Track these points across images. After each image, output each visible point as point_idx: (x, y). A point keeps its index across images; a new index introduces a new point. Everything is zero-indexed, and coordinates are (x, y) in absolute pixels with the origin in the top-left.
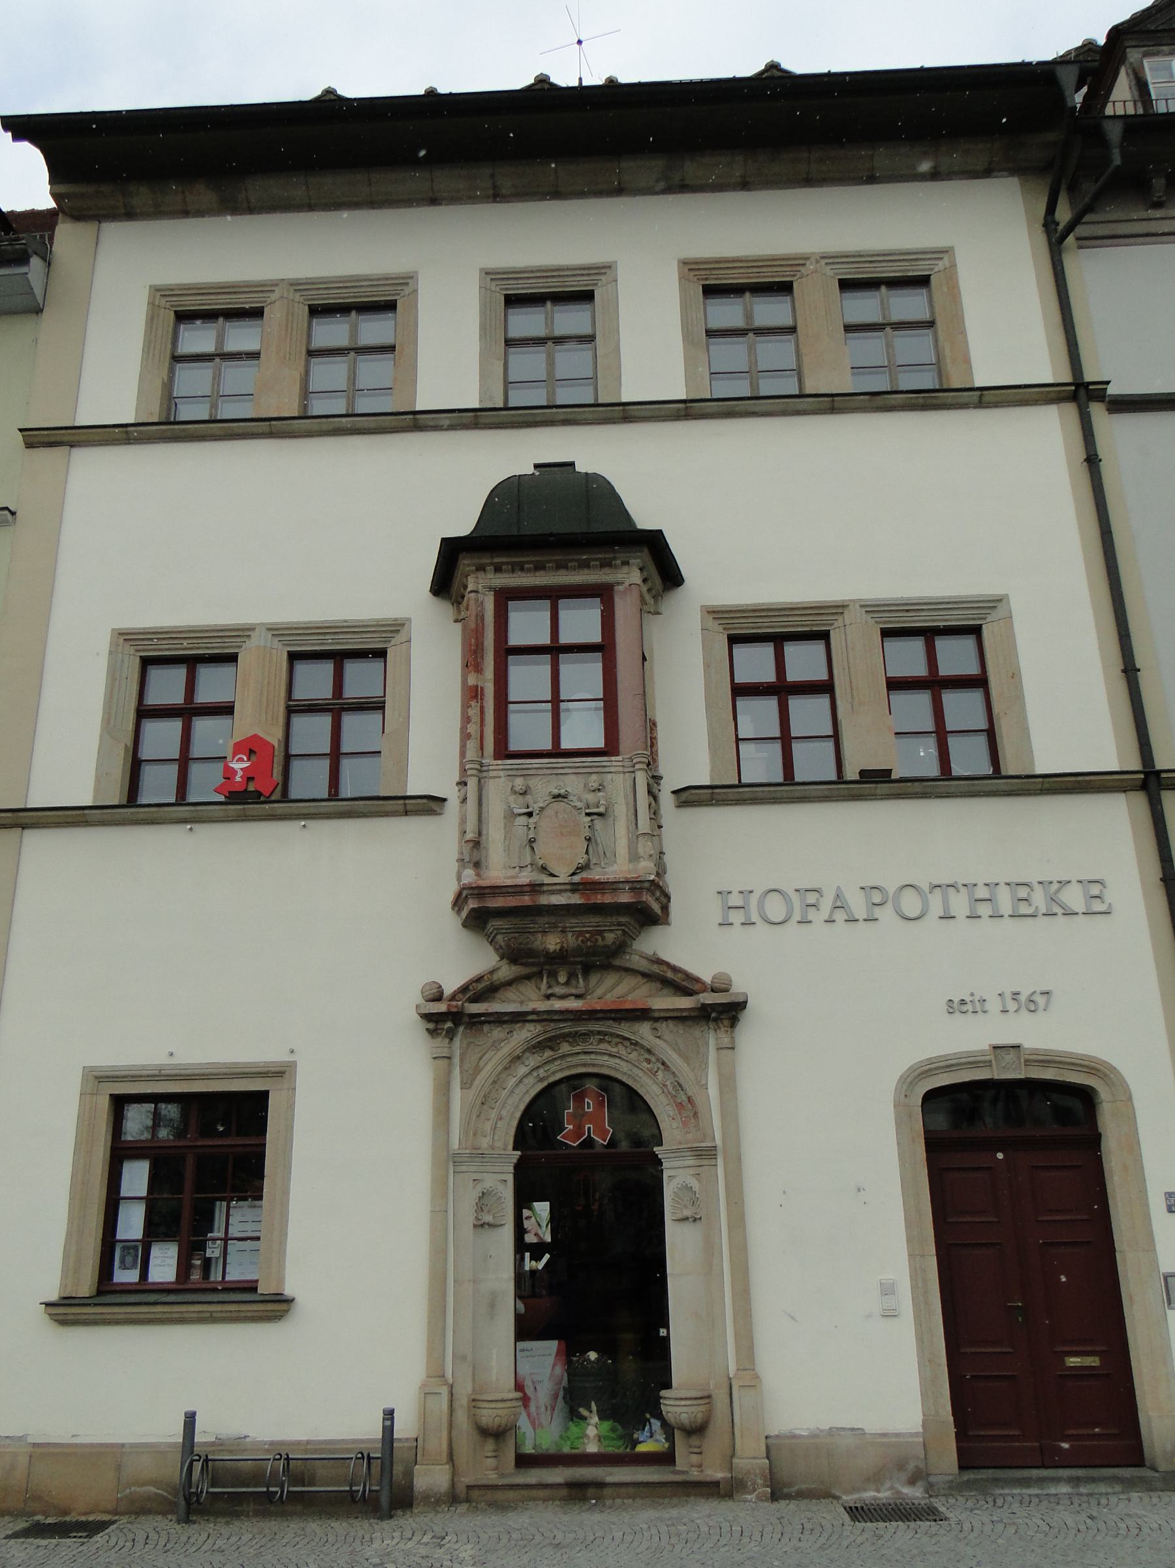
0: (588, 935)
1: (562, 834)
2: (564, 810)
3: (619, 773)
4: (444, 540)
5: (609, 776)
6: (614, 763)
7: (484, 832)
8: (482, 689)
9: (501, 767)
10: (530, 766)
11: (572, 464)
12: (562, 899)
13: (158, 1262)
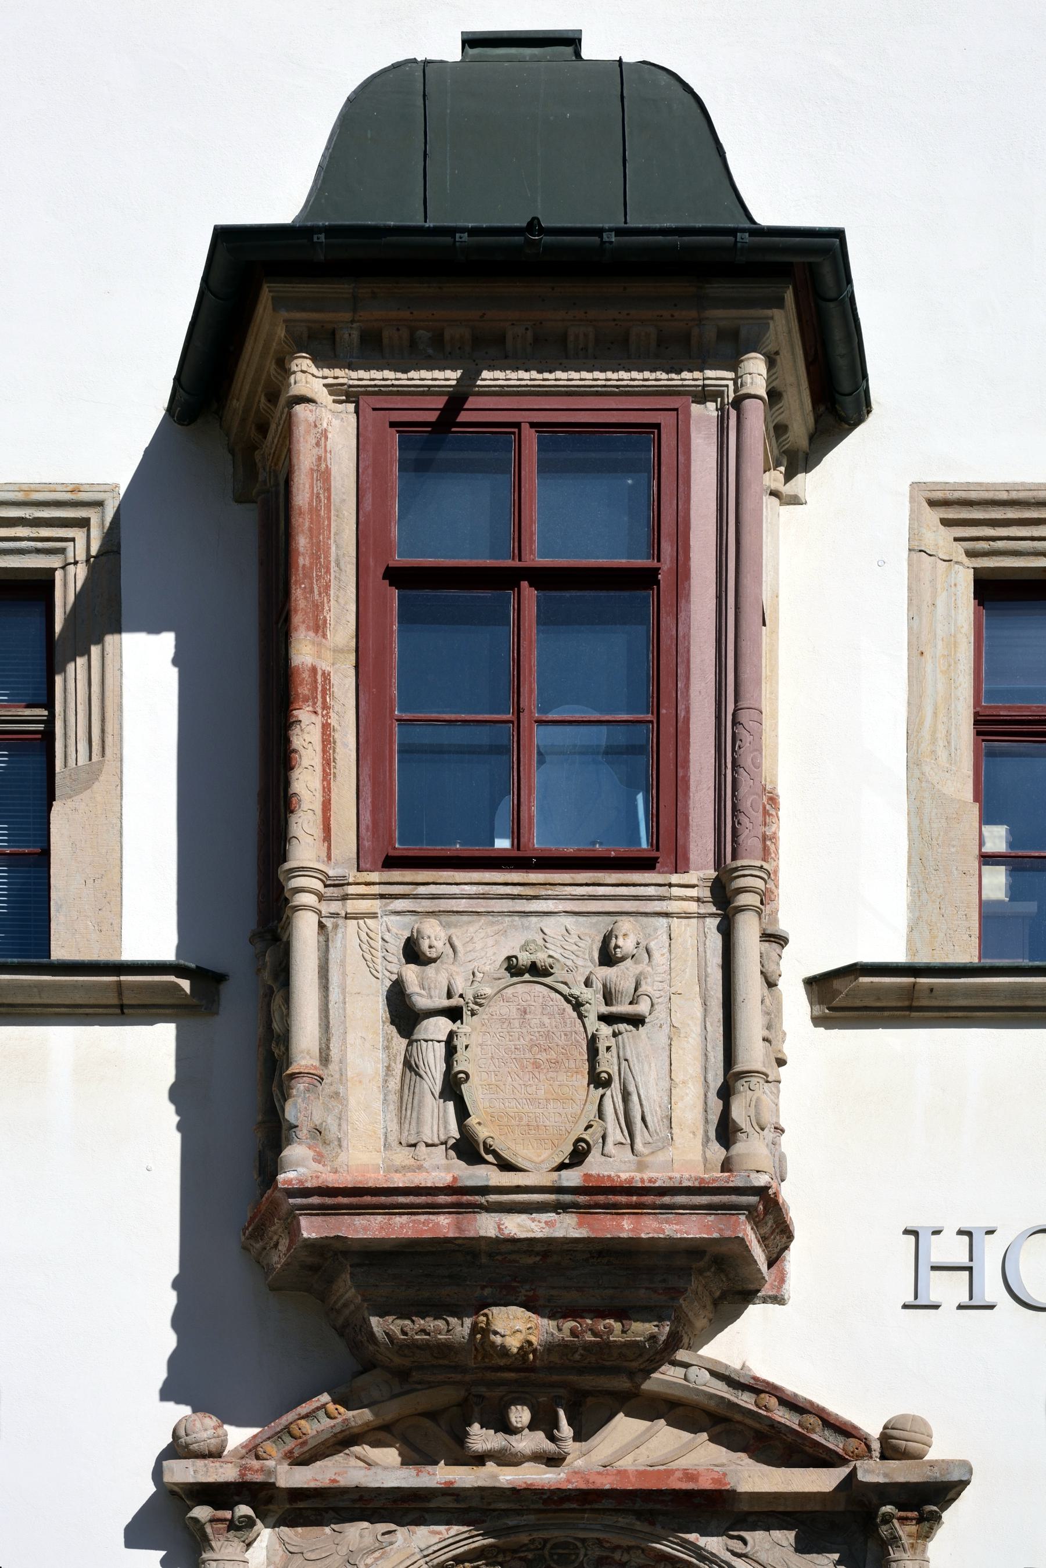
2: (544, 1006)
3: (687, 916)
4: (839, 234)
6: (676, 891)
7: (335, 1052)
8: (326, 676)
11: (571, 41)
12: (533, 1225)
13: (801, 1472)
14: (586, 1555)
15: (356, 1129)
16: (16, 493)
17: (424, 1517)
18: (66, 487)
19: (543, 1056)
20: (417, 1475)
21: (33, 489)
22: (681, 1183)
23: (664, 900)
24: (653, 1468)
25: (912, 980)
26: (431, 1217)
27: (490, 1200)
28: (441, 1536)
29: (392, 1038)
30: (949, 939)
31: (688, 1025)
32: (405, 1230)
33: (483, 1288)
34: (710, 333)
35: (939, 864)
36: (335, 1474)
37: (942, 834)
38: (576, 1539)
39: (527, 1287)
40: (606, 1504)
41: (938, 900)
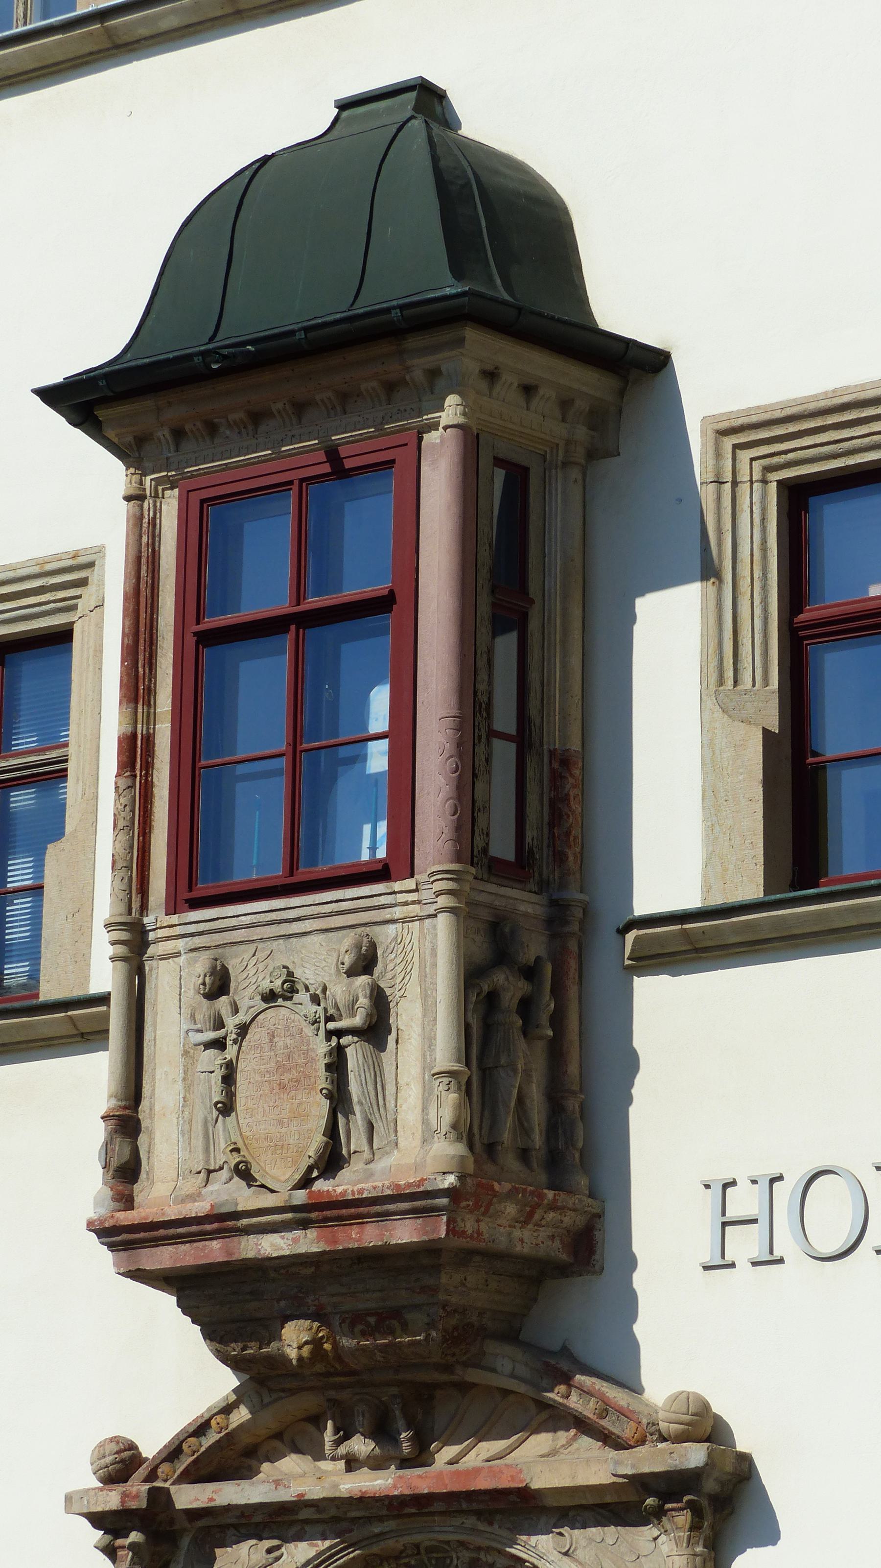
0: (372, 1320)
1: (282, 1087)
5: (392, 929)
6: (401, 898)
9: (178, 931)
10: (233, 922)
14: (458, 1558)
15: (160, 1161)
16: (34, 567)
17: (304, 1529)
18: (69, 554)
19: (286, 1077)
20: (276, 1488)
21: (46, 561)
22: (382, 1193)
23: (395, 907)
24: (490, 1463)
25: (679, 927)
26: (207, 1243)
27: (244, 1223)
28: (317, 1549)
29: (187, 1071)
30: (737, 870)
31: (411, 1026)
32: (188, 1258)
33: (278, 1301)
34: (418, 375)
35: (728, 794)
36: (213, 1492)
37: (731, 762)
38: (441, 1541)
39: (312, 1297)
40: (438, 1506)
41: (728, 832)
